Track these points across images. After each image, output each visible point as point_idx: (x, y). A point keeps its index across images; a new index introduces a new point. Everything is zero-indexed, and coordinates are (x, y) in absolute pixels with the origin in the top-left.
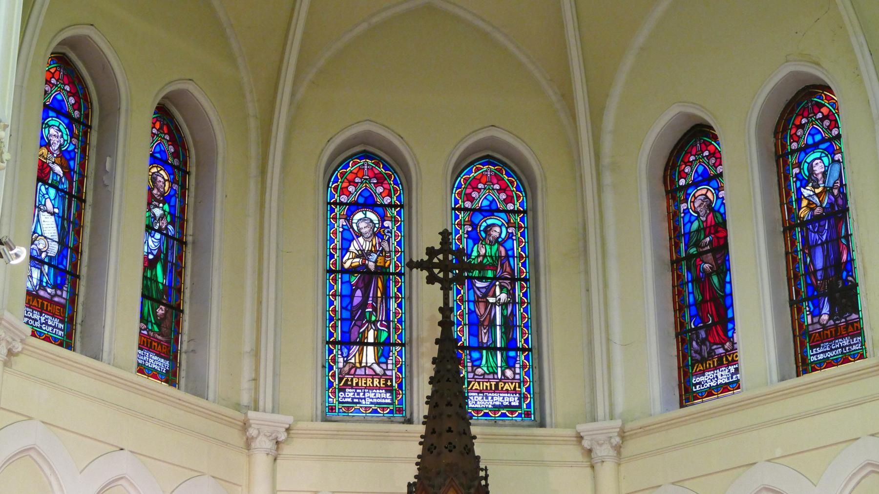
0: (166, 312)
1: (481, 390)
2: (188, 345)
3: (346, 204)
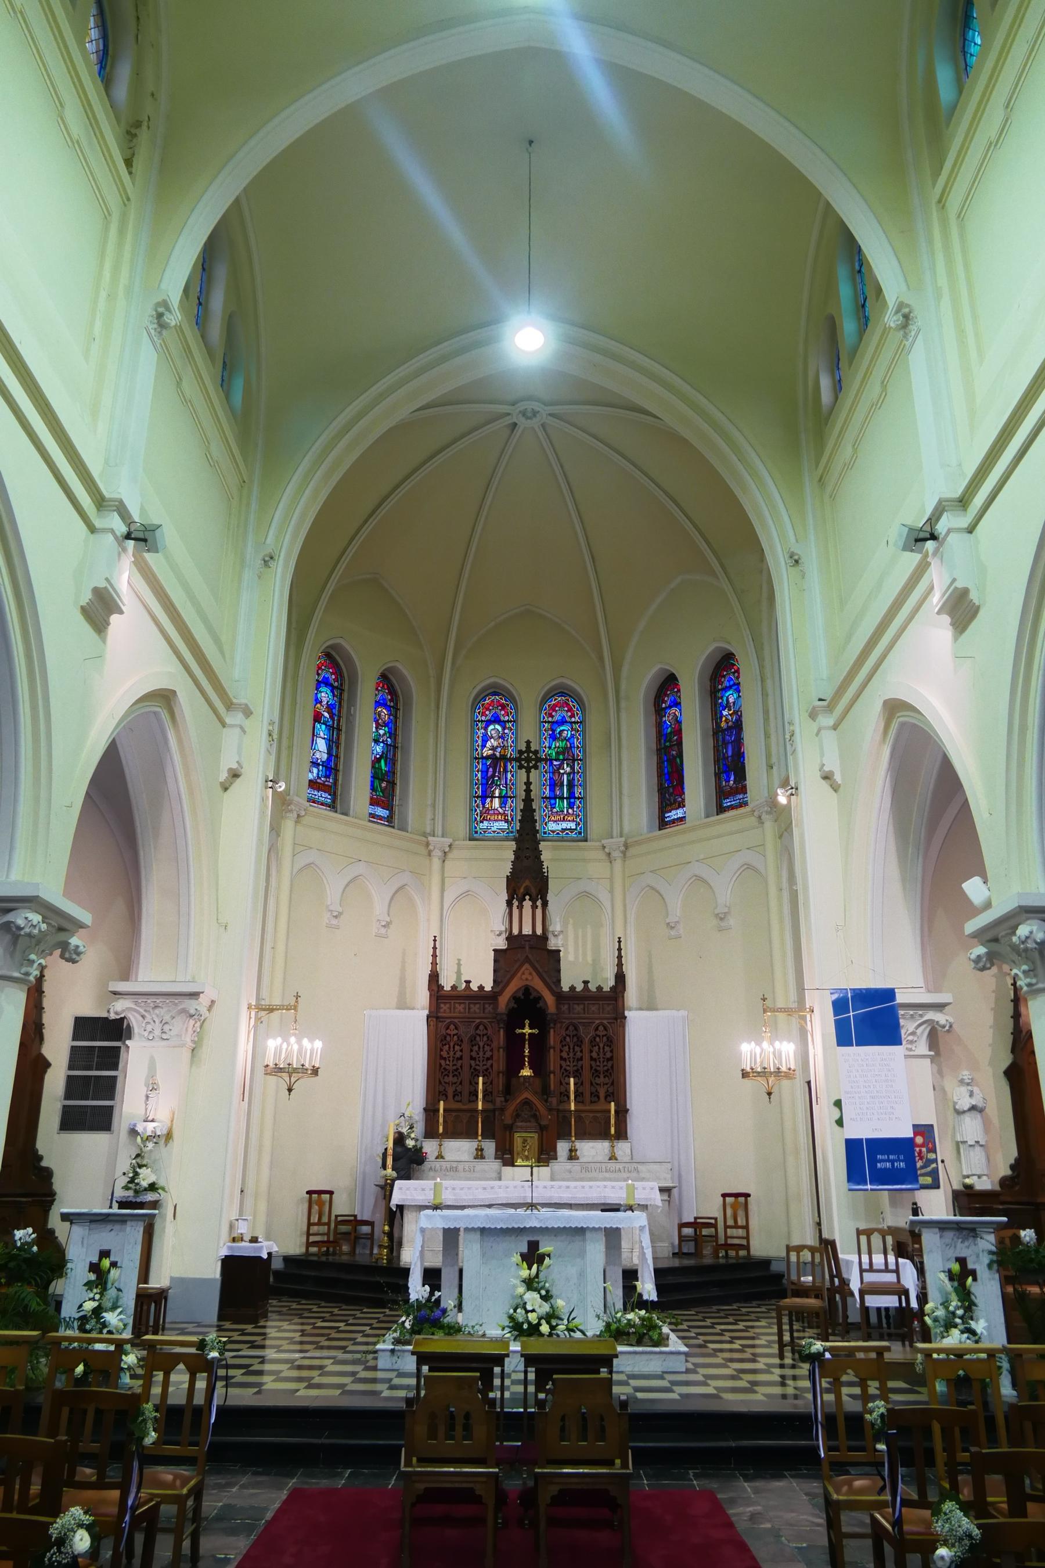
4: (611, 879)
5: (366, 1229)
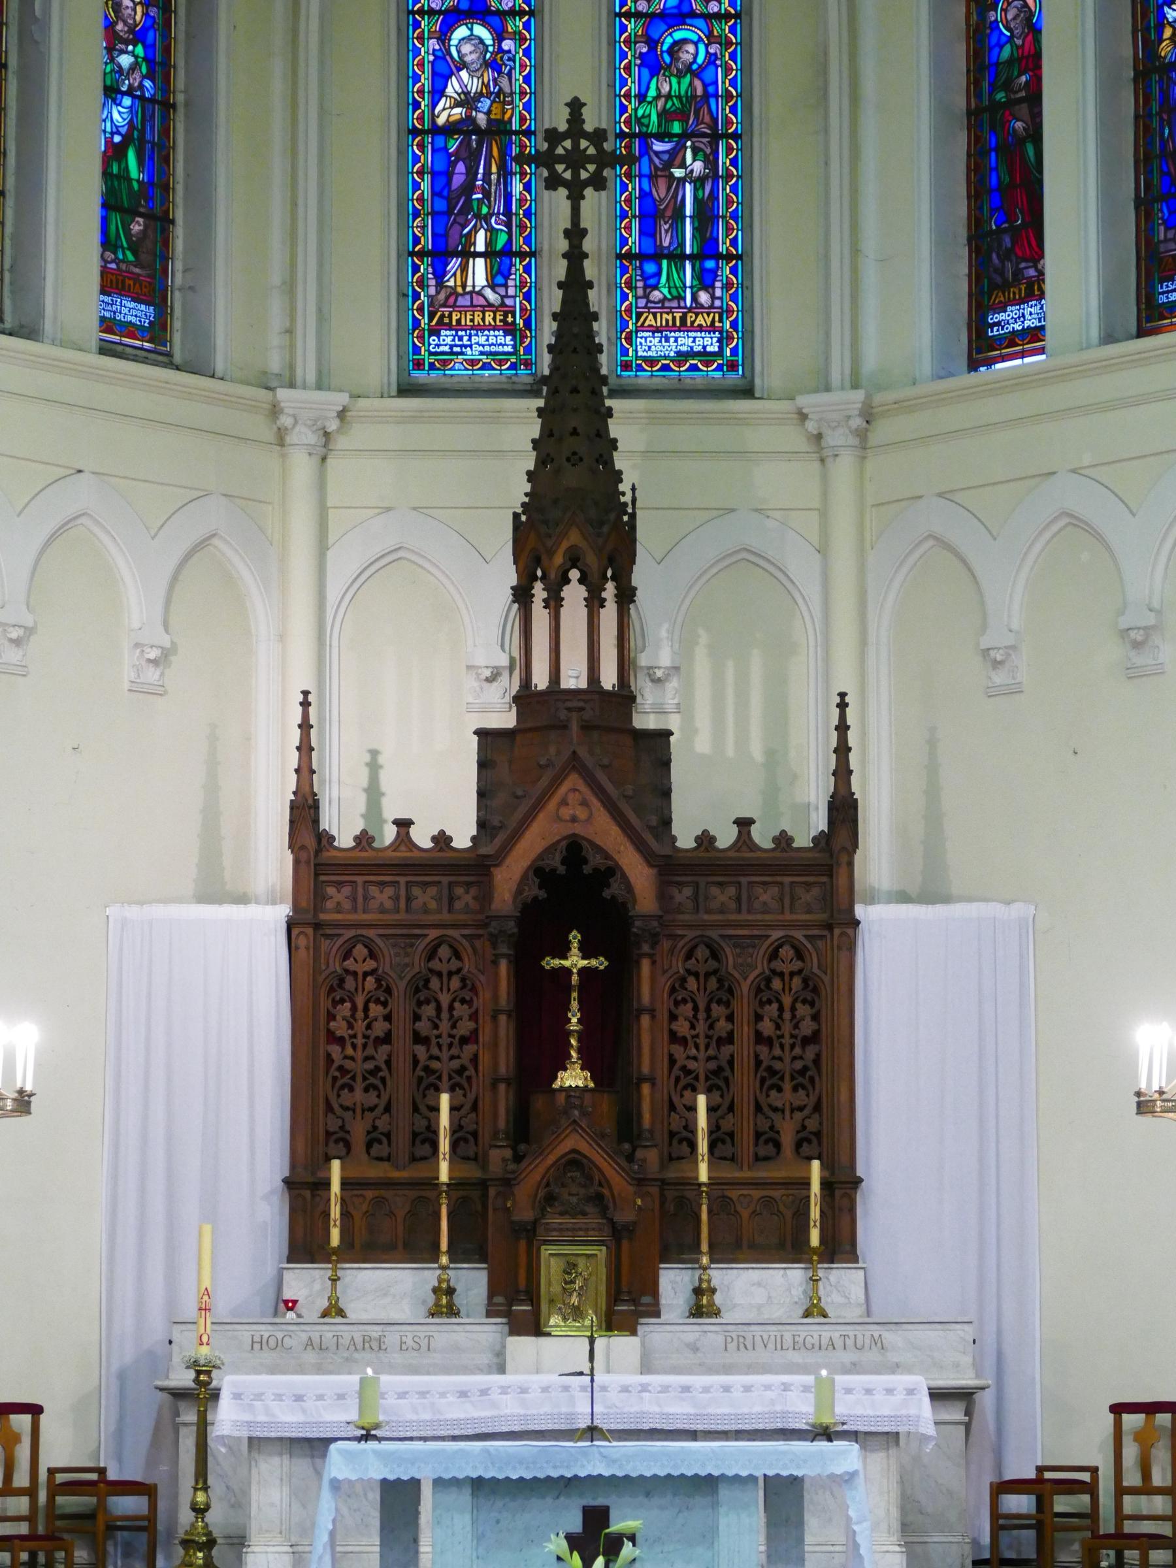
0: (146, 226)
1: (657, 327)
2: (184, 277)
3: (440, 12)
4: (824, 513)
5: (127, 1505)
